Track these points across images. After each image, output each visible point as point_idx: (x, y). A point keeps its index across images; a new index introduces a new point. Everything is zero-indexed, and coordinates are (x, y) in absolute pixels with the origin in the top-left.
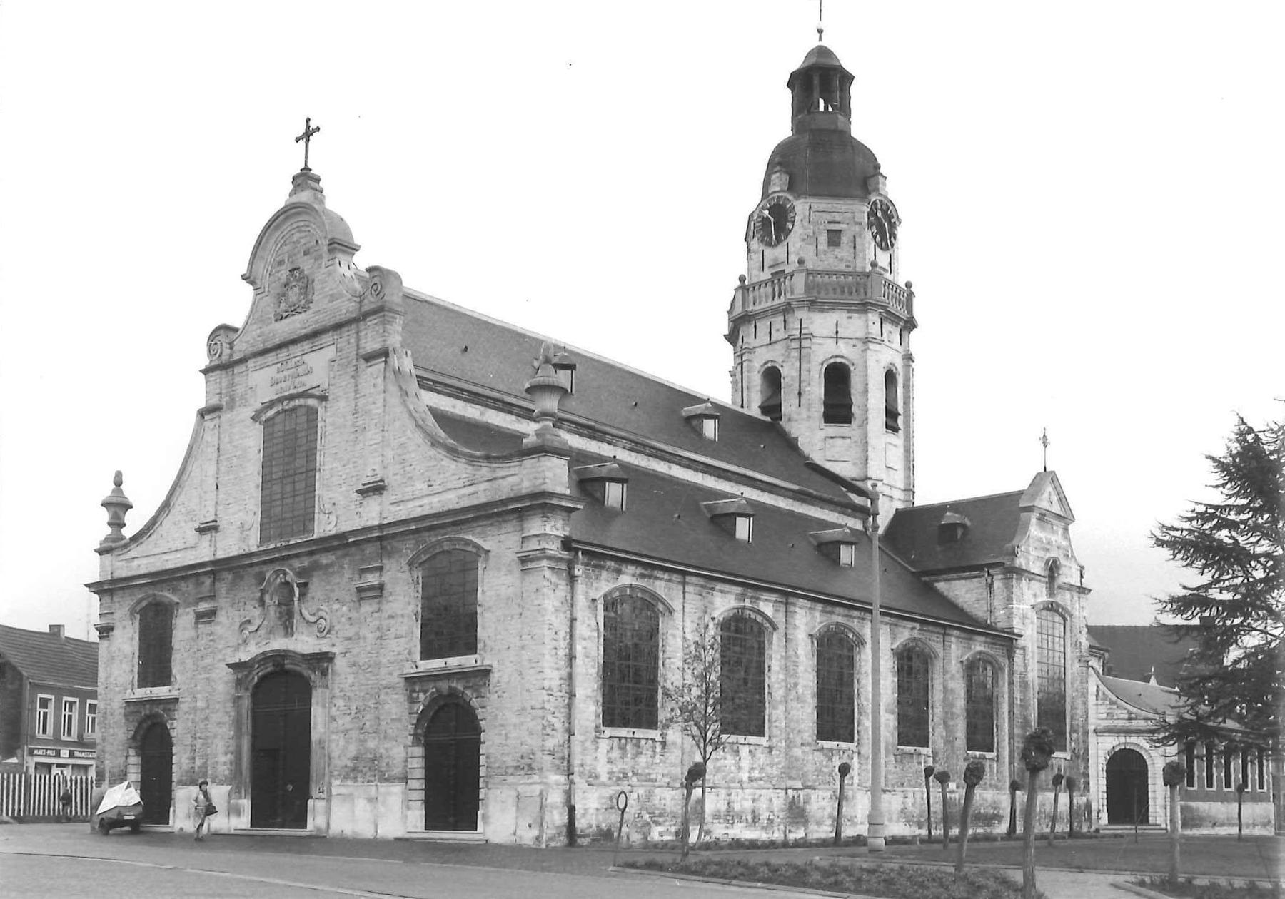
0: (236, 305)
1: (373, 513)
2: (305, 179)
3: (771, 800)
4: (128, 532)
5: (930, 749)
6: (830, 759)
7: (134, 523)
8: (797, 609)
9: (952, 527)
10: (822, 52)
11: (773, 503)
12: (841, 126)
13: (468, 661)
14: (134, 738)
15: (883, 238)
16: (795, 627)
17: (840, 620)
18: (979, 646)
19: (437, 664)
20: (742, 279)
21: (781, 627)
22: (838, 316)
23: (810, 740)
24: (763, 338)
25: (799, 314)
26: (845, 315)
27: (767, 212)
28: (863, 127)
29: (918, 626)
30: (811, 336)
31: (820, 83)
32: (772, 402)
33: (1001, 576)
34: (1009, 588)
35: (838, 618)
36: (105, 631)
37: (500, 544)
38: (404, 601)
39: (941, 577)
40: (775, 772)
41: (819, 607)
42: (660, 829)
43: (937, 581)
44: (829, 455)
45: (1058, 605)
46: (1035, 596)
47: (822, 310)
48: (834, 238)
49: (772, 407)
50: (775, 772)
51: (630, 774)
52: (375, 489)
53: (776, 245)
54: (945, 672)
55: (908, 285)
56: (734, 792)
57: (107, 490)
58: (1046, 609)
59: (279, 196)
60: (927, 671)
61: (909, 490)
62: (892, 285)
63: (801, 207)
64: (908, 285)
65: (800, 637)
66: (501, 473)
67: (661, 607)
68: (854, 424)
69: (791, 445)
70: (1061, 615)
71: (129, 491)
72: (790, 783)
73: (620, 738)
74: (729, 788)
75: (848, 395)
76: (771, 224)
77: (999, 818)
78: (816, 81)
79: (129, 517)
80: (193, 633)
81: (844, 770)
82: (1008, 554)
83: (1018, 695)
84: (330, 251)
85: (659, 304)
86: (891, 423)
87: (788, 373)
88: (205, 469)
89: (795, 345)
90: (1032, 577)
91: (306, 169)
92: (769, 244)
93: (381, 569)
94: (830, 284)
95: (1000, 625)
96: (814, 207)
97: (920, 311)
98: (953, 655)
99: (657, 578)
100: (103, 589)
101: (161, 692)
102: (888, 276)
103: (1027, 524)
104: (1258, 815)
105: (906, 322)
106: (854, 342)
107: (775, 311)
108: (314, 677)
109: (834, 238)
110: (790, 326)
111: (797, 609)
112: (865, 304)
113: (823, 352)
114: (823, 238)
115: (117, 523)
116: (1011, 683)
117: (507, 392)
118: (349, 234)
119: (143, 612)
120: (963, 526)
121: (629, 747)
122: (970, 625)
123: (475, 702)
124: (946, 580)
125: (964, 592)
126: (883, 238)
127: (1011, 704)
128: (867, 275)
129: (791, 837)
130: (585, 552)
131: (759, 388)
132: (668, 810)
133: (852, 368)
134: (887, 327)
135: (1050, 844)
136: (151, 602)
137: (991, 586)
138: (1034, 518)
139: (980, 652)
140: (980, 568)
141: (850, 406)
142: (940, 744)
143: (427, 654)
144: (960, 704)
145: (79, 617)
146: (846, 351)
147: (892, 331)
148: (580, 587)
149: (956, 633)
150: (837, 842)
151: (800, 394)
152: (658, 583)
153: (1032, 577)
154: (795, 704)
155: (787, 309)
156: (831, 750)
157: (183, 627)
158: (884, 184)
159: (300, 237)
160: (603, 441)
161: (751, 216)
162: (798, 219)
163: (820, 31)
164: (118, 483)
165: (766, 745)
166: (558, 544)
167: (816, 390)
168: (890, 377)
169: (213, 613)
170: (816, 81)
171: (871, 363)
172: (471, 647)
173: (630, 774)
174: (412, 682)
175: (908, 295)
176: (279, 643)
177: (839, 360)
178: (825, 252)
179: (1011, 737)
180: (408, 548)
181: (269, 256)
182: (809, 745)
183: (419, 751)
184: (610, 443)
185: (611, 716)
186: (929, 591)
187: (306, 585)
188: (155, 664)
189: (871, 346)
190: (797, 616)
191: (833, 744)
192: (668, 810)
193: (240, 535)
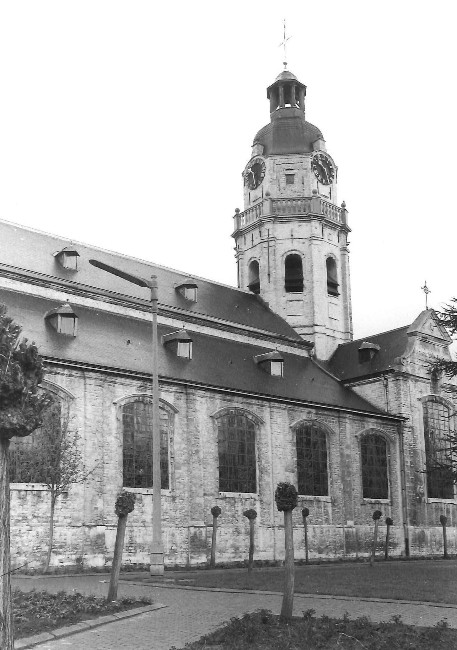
3: (173, 535)
5: (329, 497)
6: (233, 505)
8: (197, 398)
9: (368, 350)
11: (196, 330)
12: (298, 113)
15: (324, 176)
16: (195, 411)
17: (240, 406)
18: (371, 425)
20: (237, 211)
21: (183, 411)
22: (294, 225)
23: (213, 491)
24: (249, 244)
25: (267, 226)
26: (297, 224)
27: (250, 169)
29: (313, 411)
30: (275, 239)
31: (286, 92)
33: (392, 379)
34: (398, 387)
35: (237, 404)
39: (356, 383)
40: (178, 515)
41: (219, 396)
42: (60, 557)
43: (354, 386)
44: (290, 311)
45: (441, 399)
46: (421, 392)
47: (282, 222)
48: (290, 179)
49: (255, 287)
50: (179, 515)
51: (30, 517)
53: (256, 188)
54: (341, 443)
55: (343, 205)
56: (136, 529)
58: (432, 401)
60: (325, 442)
62: (334, 207)
63: (268, 162)
64: (343, 205)
65: (200, 417)
68: (306, 291)
69: (265, 307)
70: (445, 406)
72: (194, 523)
73: (20, 491)
74: (132, 526)
75: (301, 273)
76: (254, 175)
77: (395, 545)
78: (281, 90)
81: (251, 515)
82: (397, 364)
83: (408, 460)
86: (331, 290)
87: (262, 263)
89: (265, 245)
90: (417, 379)
92: (253, 189)
94: (287, 206)
95: (394, 412)
96: (277, 162)
98: (348, 431)
99: (56, 373)
102: (328, 200)
103: (412, 343)
105: (342, 227)
106: (304, 240)
107: (254, 227)
109: (290, 179)
110: (263, 235)
111: (197, 398)
112: (309, 216)
113: (284, 248)
114: (283, 179)
116: (402, 451)
120: (375, 350)
121: (29, 497)
122: (365, 410)
124: (359, 385)
125: (370, 392)
126: (324, 176)
127: (403, 465)
128: (310, 199)
129: (193, 562)
131: (248, 275)
132: (69, 542)
133: (302, 257)
134: (327, 231)
135: (371, 565)
137: (386, 386)
138: (417, 341)
139: (372, 430)
140: (378, 374)
141: (301, 280)
142: (339, 494)
144: (356, 466)
146: (299, 247)
149: (348, 416)
150: (446, 556)
151: (269, 275)
152: (59, 377)
153: (417, 379)
154: (196, 465)
155: (260, 224)
156: (234, 498)
158: (324, 145)
160: (86, 297)
161: (243, 174)
162: (267, 170)
163: (426, 290)
165: (170, 495)
167: (280, 272)
168: (331, 263)
170: (281, 90)
171: (315, 253)
173: (30, 517)
175: (343, 211)
177: (294, 252)
178: (284, 189)
179: (404, 489)
182: (212, 495)
184: (93, 298)
185: (366, 494)
186: (348, 393)
189: (314, 242)
190: (198, 403)
191: (236, 495)
192: (69, 542)
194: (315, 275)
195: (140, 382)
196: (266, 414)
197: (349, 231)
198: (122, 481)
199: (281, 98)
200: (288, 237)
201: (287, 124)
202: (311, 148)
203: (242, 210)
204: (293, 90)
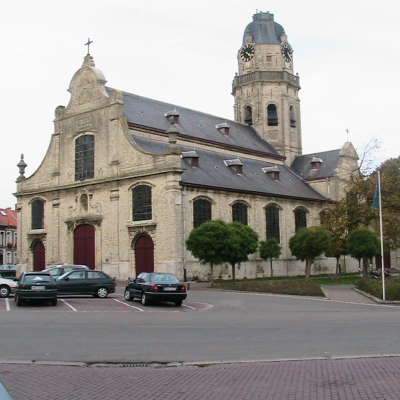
1: (116, 170)
2: (88, 58)
4: (27, 175)
36: (19, 209)
38: (126, 195)
52: (116, 163)
57: (19, 161)
59: (79, 64)
61: (300, 148)
68: (280, 125)
71: (26, 161)
76: (246, 53)
79: (26, 169)
85: (208, 90)
97: (301, 83)
100: (19, 196)
104: (8, 308)
108: (96, 227)
114: (265, 58)
115: (22, 172)
117: (159, 125)
119: (33, 204)
123: (152, 235)
136: (36, 201)
143: (136, 218)
145: (11, 202)
146: (276, 101)
147: (291, 91)
157: (48, 207)
164: (22, 158)
167: (265, 114)
169: (58, 204)
172: (150, 217)
174: (130, 229)
175: (298, 78)
176: (84, 214)
183: (133, 251)
188: (38, 219)
194: (283, 114)
196: (282, 205)
198: (97, 233)
200: (271, 93)
201: (263, 30)
202: (279, 39)
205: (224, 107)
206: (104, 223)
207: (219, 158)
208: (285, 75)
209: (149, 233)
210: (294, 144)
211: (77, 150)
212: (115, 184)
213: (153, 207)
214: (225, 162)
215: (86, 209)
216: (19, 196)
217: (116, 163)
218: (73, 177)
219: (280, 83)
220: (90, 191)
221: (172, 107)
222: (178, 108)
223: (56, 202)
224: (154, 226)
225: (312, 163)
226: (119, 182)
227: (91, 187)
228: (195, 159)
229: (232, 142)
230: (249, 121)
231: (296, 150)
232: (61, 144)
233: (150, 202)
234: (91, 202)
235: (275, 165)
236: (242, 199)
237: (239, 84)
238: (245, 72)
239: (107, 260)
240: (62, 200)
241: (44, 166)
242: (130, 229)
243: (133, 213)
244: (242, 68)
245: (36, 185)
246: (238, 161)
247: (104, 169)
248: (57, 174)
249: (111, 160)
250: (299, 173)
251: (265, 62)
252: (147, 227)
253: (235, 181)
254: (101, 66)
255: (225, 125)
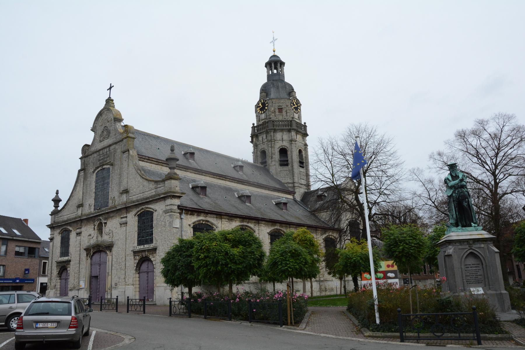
0: (89, 138)
2: (109, 101)
7: (61, 205)
10: (274, 56)
13: (151, 246)
14: (58, 274)
19: (142, 247)
20: (253, 124)
28: (288, 78)
31: (275, 64)
32: (264, 161)
35: (277, 227)
36: (52, 239)
37: (158, 208)
38: (132, 219)
52: (126, 191)
55: (305, 123)
57: (54, 196)
59: (102, 105)
61: (308, 185)
64: (305, 123)
66: (159, 186)
67: (214, 227)
71: (60, 196)
78: (273, 65)
80: (75, 239)
84: (115, 121)
87: (269, 151)
88: (80, 188)
91: (110, 97)
93: (126, 217)
100: (52, 227)
101: (66, 258)
113: (278, 145)
114: (277, 111)
115: (56, 206)
118: (120, 115)
123: (152, 259)
130: (185, 210)
143: (140, 243)
146: (286, 144)
147: (299, 137)
148: (184, 221)
157: (73, 236)
159: (107, 118)
163: (274, 51)
164: (57, 192)
166: (176, 207)
167: (277, 156)
168: (300, 151)
170: (273, 65)
174: (135, 253)
175: (305, 126)
180: (134, 212)
181: (100, 122)
187: (106, 223)
189: (293, 142)
193: (89, 209)
194: (294, 156)
195: (65, 218)
197: (307, 135)
199: (273, 68)
200: (281, 139)
203: (255, 125)
204: (279, 65)
205: (244, 151)
206: (114, 249)
207: (229, 190)
208: (294, 123)
209: (151, 257)
210: (304, 182)
211: (96, 182)
212: (124, 211)
213: (155, 231)
214: (236, 194)
215: (102, 237)
216: (52, 227)
217: (126, 191)
218: (93, 207)
219: (289, 131)
220: (105, 219)
221: (238, 160)
222: (194, 147)
223: (78, 231)
224: (154, 250)
225: (318, 196)
226: (127, 209)
227: (106, 216)
228: (204, 188)
229: (245, 178)
230: (264, 163)
231: (305, 187)
232: (85, 178)
233: (152, 227)
234: (106, 229)
235: (284, 197)
236: (245, 224)
237: (257, 133)
238: (261, 123)
239: (116, 284)
240: (83, 229)
241: (72, 199)
242: (135, 253)
243: (138, 238)
244: (258, 119)
245: (66, 216)
246: (201, 183)
247: (116, 198)
248: (80, 206)
249: (122, 189)
250: (307, 206)
251: (277, 113)
252: (149, 251)
253: (243, 209)
254: (118, 106)
255: (240, 164)
